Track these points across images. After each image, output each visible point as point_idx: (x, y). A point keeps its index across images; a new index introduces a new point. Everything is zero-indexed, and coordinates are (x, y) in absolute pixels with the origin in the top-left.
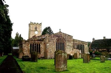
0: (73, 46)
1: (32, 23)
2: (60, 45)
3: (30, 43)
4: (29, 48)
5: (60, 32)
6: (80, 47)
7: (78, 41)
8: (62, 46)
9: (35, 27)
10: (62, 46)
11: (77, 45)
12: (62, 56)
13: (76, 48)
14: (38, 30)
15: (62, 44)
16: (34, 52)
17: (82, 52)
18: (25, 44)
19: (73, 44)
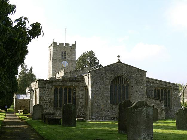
7: (158, 82)
8: (123, 92)
9: (62, 53)
10: (123, 92)
11: (155, 90)
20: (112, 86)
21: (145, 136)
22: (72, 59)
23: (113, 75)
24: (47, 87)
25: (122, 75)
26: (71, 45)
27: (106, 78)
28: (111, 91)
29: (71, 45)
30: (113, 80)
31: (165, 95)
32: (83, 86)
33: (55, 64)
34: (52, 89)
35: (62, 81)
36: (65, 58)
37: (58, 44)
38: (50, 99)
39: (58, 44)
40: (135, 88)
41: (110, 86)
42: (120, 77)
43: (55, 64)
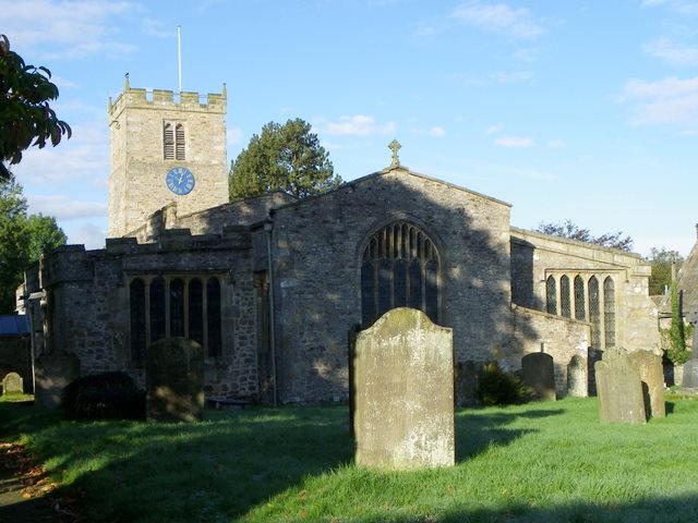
3: (129, 271)
12: (407, 353)
14: (199, 158)
18: (80, 282)
21: (423, 439)
22: (213, 157)
23: (372, 220)
24: (96, 279)
25: (412, 223)
27: (341, 233)
32: (249, 271)
33: (137, 182)
34: (118, 286)
35: (160, 253)
38: (111, 326)
41: (360, 265)
43: (137, 182)
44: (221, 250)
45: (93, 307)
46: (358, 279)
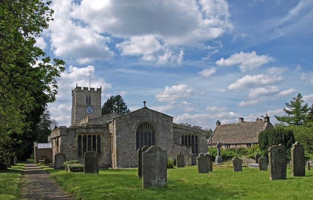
0: (174, 139)
1: (80, 88)
2: (146, 137)
4: (76, 145)
5: (145, 108)
6: (189, 141)
9: (87, 98)
11: (183, 136)
12: (156, 157)
13: (179, 144)
14: (94, 104)
15: (150, 135)
16: (91, 153)
17: (193, 152)
19: (174, 135)
20: (137, 133)
26: (96, 90)
28: (137, 139)
29: (96, 90)
30: (139, 126)
31: (193, 141)
36: (90, 103)
37: (82, 89)
38: (73, 147)
39: (82, 89)
40: (161, 134)
42: (146, 123)
44: (101, 128)
45: (68, 142)
46: (135, 136)
